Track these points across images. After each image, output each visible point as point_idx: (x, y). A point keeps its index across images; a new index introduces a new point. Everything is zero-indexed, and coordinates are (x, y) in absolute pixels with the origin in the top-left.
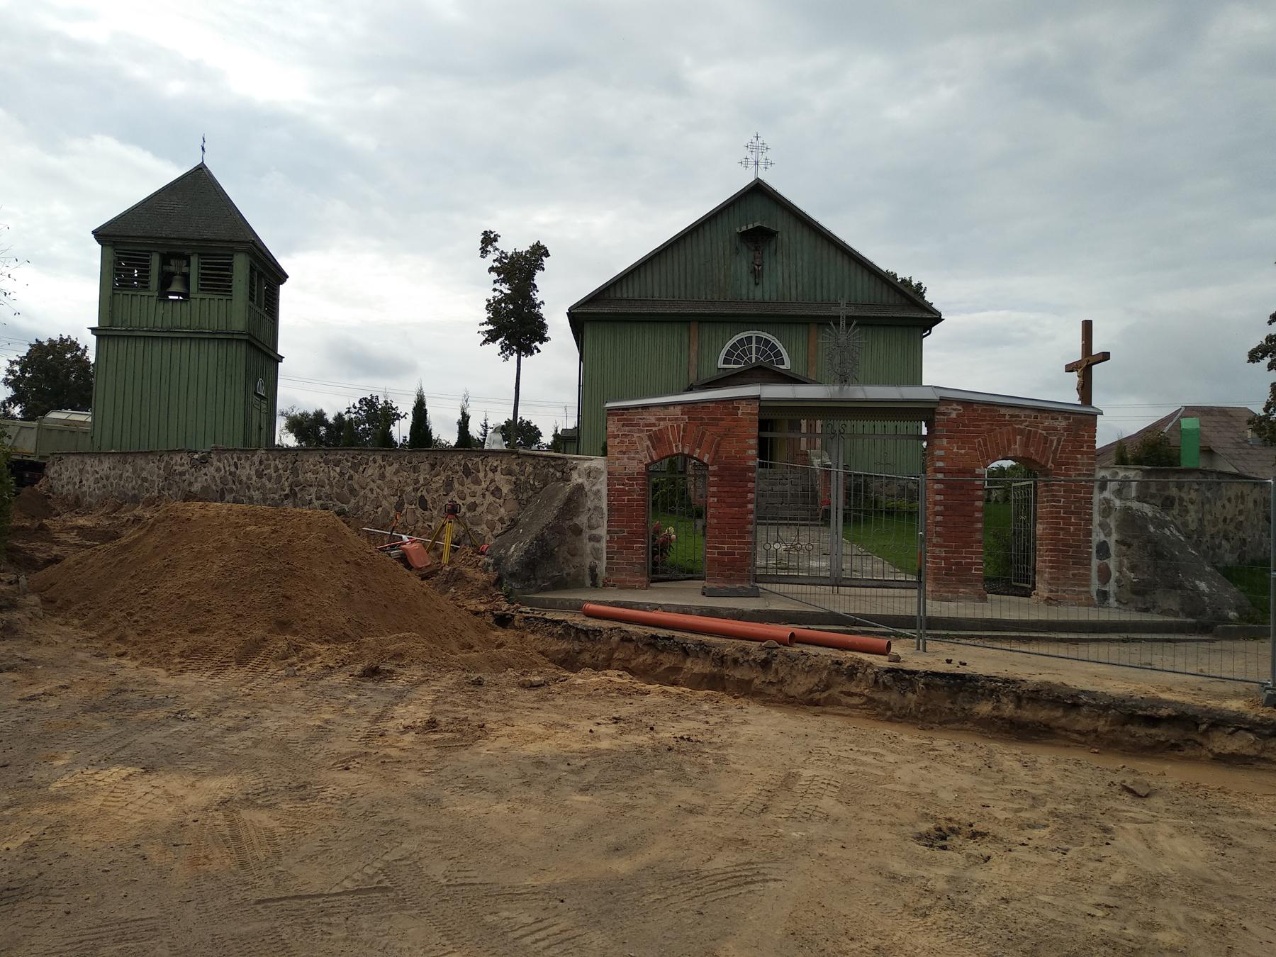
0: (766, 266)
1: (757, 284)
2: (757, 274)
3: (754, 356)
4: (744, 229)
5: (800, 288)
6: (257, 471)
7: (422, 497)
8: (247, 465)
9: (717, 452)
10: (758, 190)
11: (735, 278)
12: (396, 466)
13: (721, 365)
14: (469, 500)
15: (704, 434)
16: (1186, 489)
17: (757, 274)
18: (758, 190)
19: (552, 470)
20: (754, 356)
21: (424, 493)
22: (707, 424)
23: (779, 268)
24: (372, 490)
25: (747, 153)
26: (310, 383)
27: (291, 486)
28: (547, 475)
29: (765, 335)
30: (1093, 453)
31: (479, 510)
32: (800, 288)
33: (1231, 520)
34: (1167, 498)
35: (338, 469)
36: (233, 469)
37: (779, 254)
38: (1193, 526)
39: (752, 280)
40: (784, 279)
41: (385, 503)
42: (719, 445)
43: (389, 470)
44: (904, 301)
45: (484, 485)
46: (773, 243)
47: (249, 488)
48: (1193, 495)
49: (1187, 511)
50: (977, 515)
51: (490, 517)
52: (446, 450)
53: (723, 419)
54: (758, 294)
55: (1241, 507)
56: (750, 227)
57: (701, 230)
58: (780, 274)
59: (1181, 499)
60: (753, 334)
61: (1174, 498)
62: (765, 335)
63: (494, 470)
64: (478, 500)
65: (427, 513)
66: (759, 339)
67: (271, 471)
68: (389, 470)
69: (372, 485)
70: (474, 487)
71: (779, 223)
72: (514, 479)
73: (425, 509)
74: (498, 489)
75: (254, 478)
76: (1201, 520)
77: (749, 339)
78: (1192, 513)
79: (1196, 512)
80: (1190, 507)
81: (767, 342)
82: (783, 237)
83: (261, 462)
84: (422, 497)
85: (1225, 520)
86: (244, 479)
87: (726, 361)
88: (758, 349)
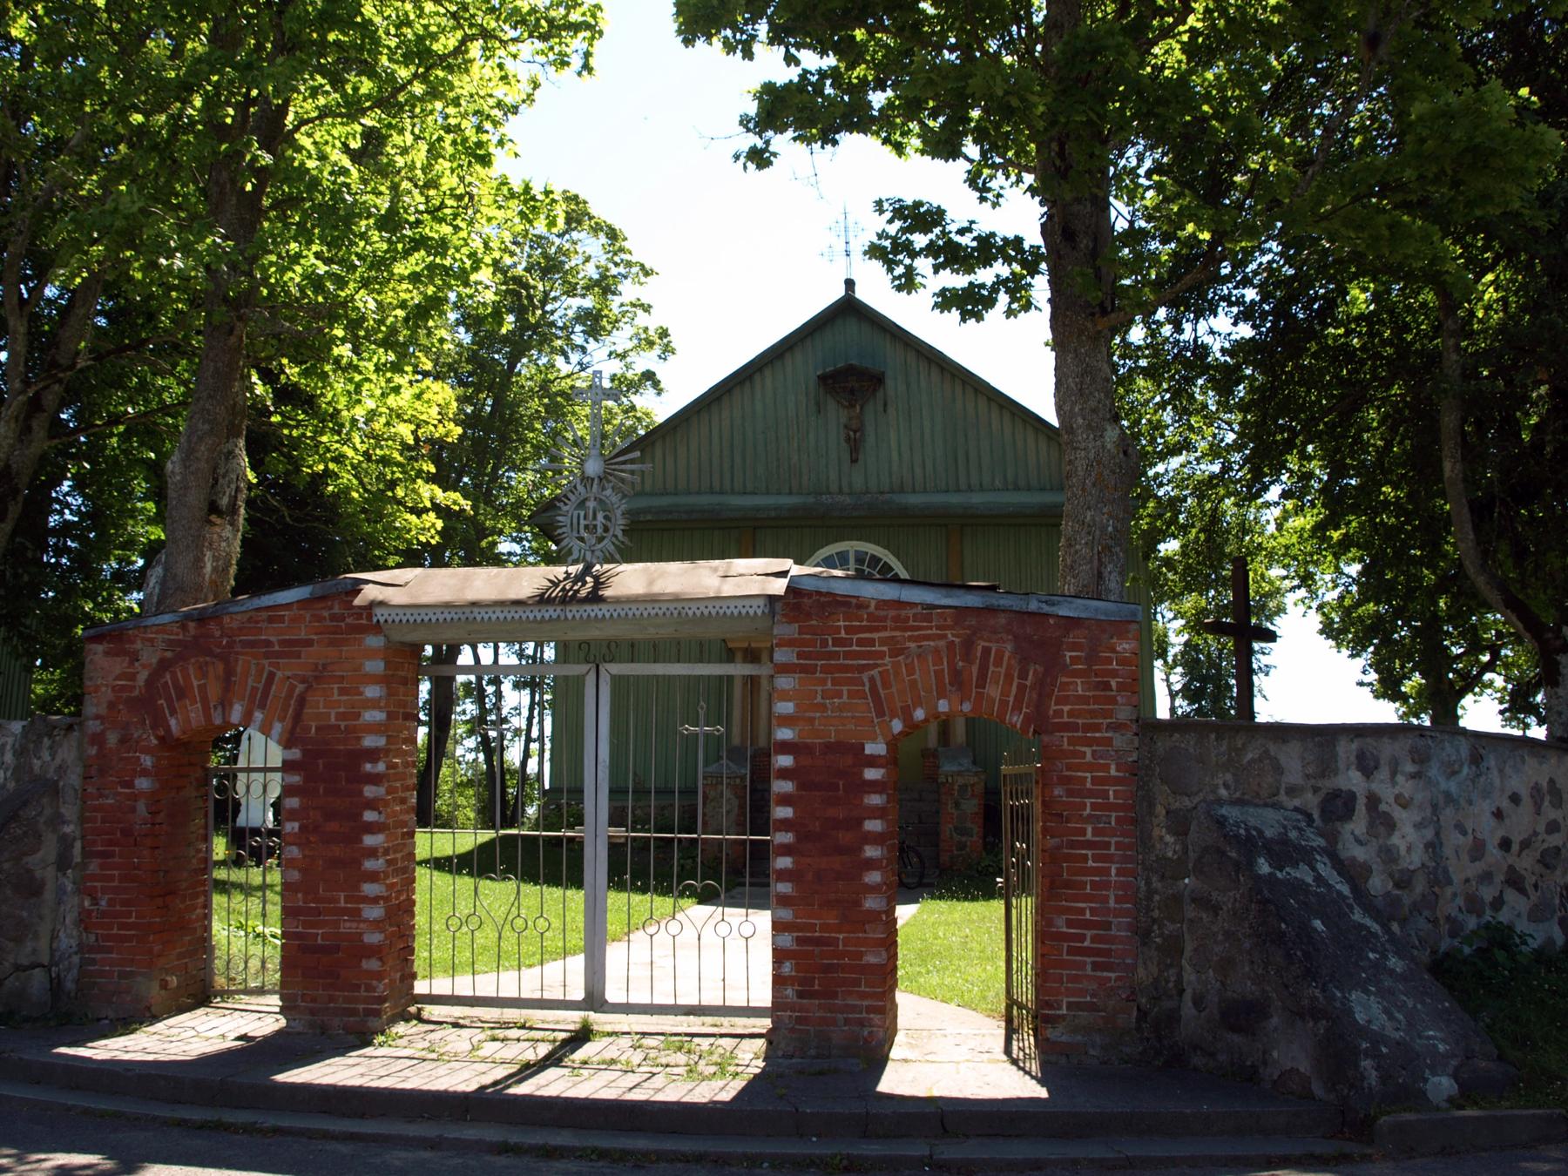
0: (870, 429)
1: (854, 461)
2: (855, 446)
16: (1384, 773)
17: (855, 446)
23: (893, 435)
26: (1260, 719)
30: (364, 556)
33: (1525, 844)
34: (1336, 794)
37: (891, 410)
38: (1415, 859)
39: (846, 457)
42: (302, 702)
46: (880, 394)
48: (1405, 786)
50: (871, 852)
53: (309, 643)
55: (1552, 814)
58: (894, 445)
59: (1373, 801)
61: (1352, 797)
76: (1433, 847)
78: (1408, 830)
79: (1418, 826)
80: (1398, 813)
81: (875, 560)
85: (1505, 844)
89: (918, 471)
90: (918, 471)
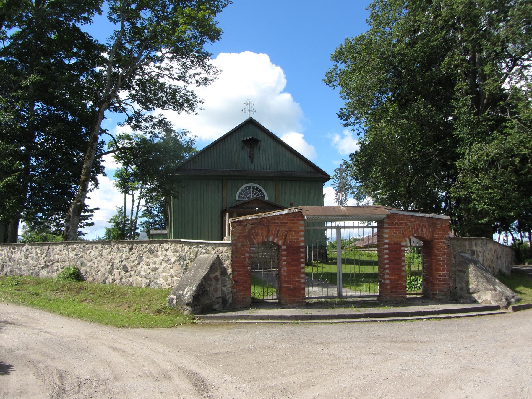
1: (252, 163)
2: (252, 159)
3: (252, 194)
4: (245, 139)
5: (270, 165)
6: (25, 255)
7: (125, 265)
8: (19, 253)
9: (285, 239)
10: (251, 122)
11: (241, 159)
12: (109, 250)
13: (237, 198)
14: (152, 266)
15: (279, 231)
17: (252, 159)
18: (251, 122)
19: (200, 249)
20: (252, 194)
21: (126, 263)
22: (280, 226)
24: (94, 263)
25: (245, 106)
27: (45, 262)
28: (197, 252)
29: (256, 185)
31: (158, 271)
32: (270, 165)
35: (74, 253)
36: (10, 254)
37: (261, 150)
40: (264, 160)
41: (103, 269)
42: (286, 236)
43: (105, 252)
44: (314, 171)
45: (161, 258)
47: (19, 264)
48: (480, 249)
49: (479, 256)
51: (164, 274)
52: (495, 242)
53: (288, 223)
54: (252, 167)
56: (248, 138)
57: (226, 139)
58: (261, 159)
60: (251, 185)
62: (256, 185)
63: (167, 250)
64: (157, 266)
65: (127, 273)
66: (253, 187)
67: (34, 255)
68: (105, 252)
69: (95, 260)
70: (155, 259)
71: (261, 136)
72: (178, 254)
73: (127, 271)
74: (169, 259)
75: (23, 259)
76: (483, 260)
77: (249, 187)
81: (257, 188)
82: (262, 143)
83: (27, 250)
84: (125, 265)
86: (16, 259)
87: (239, 197)
88: (253, 191)
89: (268, 166)
90: (268, 166)
